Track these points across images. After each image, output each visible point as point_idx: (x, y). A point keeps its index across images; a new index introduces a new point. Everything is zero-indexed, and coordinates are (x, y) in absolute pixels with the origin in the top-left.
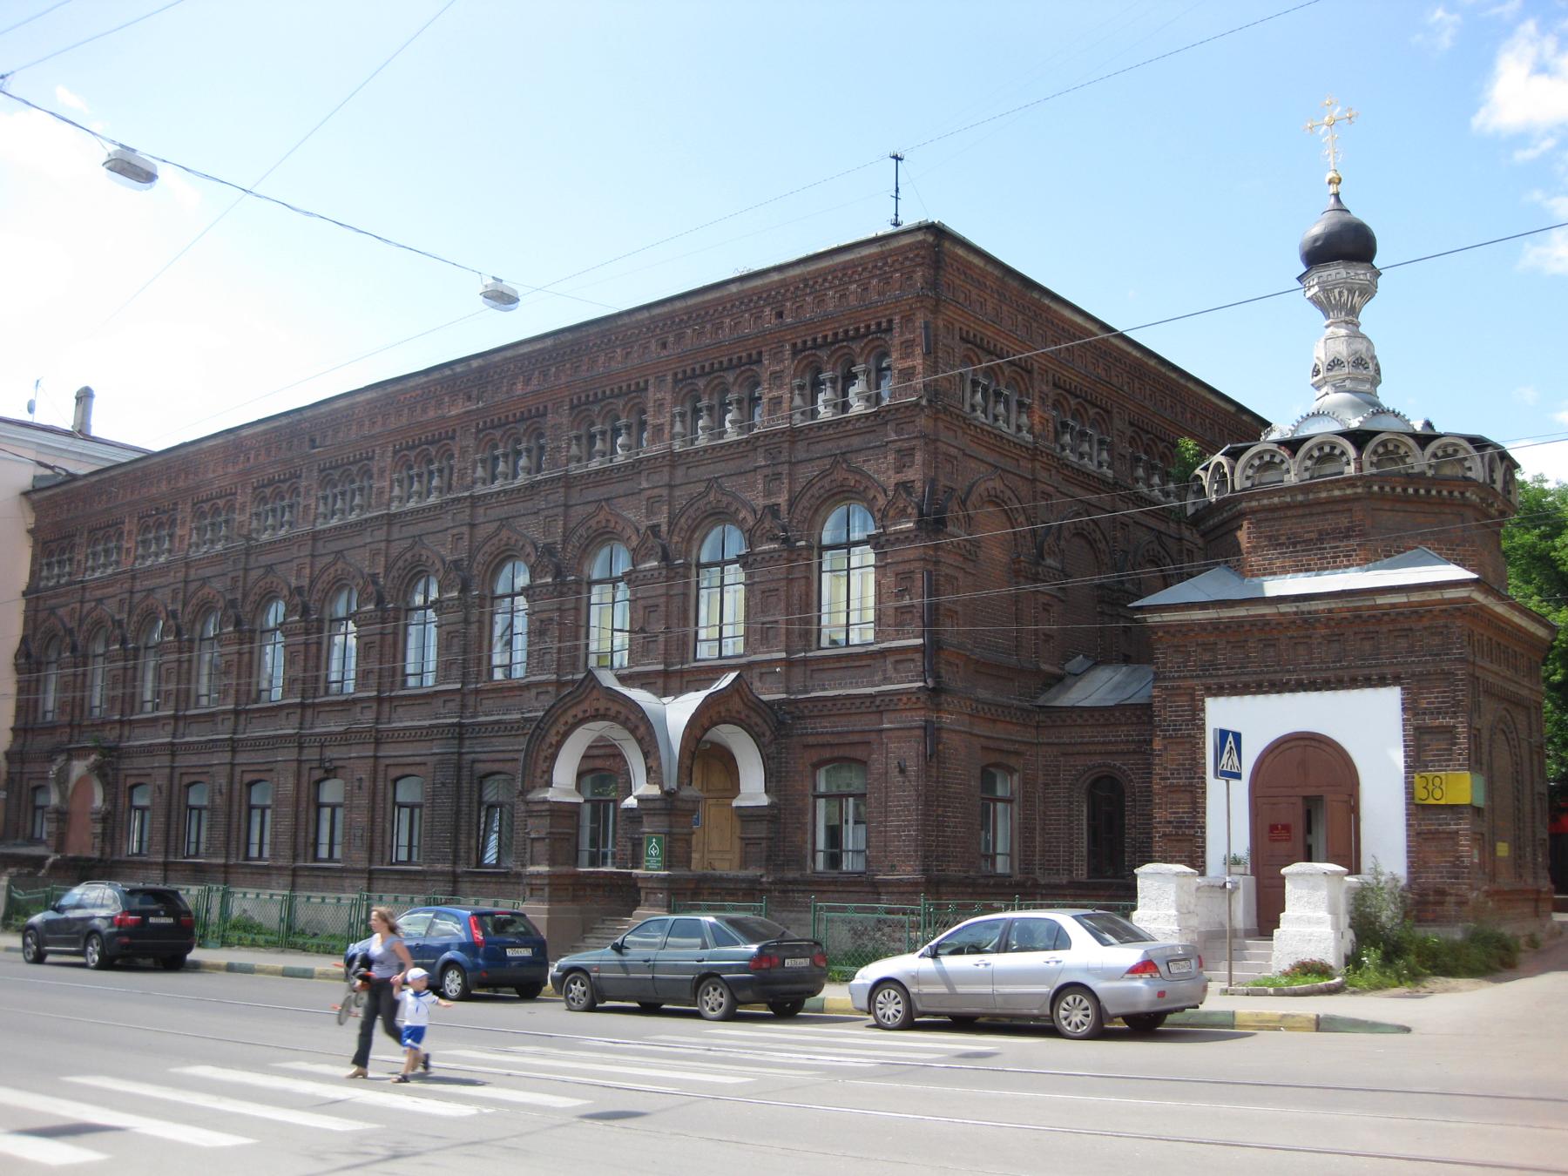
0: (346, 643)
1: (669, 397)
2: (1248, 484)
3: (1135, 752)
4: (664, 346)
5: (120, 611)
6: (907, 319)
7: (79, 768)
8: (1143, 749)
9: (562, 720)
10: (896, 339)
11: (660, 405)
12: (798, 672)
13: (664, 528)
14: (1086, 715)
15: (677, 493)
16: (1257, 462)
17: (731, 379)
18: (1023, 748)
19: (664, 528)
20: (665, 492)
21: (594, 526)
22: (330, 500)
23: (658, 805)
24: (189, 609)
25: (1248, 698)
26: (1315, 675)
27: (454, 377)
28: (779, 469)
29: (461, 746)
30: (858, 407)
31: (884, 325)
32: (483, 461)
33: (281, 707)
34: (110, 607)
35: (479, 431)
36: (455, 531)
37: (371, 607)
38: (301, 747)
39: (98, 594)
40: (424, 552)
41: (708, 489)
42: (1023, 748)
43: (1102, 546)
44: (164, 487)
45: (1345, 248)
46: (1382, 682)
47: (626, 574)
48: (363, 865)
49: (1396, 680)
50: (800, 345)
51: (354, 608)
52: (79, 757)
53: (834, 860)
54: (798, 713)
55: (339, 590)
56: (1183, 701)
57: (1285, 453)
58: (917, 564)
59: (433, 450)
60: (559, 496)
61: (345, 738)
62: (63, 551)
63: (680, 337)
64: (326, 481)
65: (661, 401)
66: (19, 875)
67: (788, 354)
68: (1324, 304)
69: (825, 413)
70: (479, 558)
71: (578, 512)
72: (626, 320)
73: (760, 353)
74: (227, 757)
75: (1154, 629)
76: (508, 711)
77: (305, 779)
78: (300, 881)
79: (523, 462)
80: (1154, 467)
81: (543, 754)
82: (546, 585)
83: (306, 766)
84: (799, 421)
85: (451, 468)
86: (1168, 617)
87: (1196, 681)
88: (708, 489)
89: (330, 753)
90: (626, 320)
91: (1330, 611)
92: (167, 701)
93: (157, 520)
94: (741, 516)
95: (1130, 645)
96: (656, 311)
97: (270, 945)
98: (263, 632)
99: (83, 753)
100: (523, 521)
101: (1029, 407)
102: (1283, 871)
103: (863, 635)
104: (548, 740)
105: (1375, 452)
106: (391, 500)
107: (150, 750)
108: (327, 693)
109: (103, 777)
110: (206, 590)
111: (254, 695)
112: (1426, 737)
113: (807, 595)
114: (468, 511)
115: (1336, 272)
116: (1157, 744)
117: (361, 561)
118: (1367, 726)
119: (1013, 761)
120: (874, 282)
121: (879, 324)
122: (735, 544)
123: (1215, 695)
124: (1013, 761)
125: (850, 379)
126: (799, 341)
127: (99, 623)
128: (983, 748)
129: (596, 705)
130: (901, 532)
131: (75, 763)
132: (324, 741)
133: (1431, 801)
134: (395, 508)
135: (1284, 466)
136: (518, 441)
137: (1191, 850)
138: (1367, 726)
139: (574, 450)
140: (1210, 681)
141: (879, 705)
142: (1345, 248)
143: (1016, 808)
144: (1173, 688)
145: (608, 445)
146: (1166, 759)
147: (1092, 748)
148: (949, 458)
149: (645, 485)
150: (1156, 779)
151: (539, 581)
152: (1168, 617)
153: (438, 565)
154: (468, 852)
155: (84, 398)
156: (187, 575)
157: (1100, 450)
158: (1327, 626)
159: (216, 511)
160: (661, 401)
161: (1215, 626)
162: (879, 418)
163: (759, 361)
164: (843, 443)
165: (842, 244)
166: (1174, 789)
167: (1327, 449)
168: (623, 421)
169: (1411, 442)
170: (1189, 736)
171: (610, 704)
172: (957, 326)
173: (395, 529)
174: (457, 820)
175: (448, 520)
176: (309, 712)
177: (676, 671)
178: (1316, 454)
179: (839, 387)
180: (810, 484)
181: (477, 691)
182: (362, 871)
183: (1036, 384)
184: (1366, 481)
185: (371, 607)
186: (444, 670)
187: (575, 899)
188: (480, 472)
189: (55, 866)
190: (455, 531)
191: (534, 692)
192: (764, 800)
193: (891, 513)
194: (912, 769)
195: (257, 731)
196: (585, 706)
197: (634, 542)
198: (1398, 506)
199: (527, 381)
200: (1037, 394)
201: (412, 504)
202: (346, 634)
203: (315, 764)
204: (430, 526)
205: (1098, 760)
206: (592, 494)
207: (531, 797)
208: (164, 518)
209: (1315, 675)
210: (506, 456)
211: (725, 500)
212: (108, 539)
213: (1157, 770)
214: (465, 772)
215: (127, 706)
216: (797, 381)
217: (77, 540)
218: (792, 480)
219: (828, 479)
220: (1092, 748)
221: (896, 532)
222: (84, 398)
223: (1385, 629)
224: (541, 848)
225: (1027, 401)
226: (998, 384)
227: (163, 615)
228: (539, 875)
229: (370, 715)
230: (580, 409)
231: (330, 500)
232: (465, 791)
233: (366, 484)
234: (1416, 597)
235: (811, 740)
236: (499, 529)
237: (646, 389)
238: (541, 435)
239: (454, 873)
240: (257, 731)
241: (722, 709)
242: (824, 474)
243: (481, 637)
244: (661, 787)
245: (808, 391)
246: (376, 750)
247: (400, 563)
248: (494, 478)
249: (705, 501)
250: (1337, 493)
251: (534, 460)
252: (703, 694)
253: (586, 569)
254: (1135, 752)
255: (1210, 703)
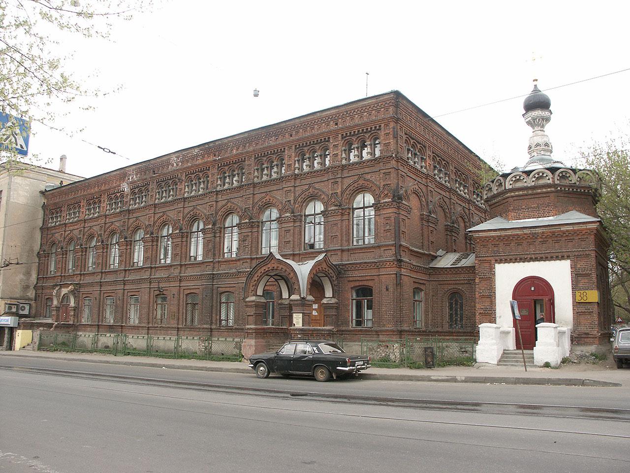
0: (115, 252)
1: (293, 154)
2: (511, 187)
3: (467, 283)
4: (291, 136)
5: (79, 235)
6: (387, 125)
7: (64, 291)
8: (471, 283)
9: (259, 271)
10: (382, 133)
11: (213, 175)
12: (345, 254)
13: (292, 202)
14: (448, 270)
15: (297, 189)
16: (514, 179)
17: (318, 148)
18: (425, 282)
19: (292, 202)
20: (292, 189)
21: (265, 201)
22: (161, 193)
23: (299, 302)
24: (107, 233)
25: (553, 262)
26: (537, 256)
27: (210, 148)
28: (337, 180)
29: (213, 282)
30: (235, 184)
31: (327, 139)
32: (220, 178)
33: (142, 268)
34: (76, 232)
35: (219, 168)
36: (210, 204)
37: (178, 231)
38: (150, 283)
39: (71, 228)
40: (198, 211)
41: (310, 187)
42: (425, 282)
43: (447, 211)
44: (96, 189)
45: (537, 104)
46: (563, 258)
47: (277, 218)
48: (175, 326)
49: (568, 257)
50: (345, 135)
51: (117, 241)
52: (64, 287)
53: (359, 323)
54: (346, 269)
55: (165, 225)
56: (487, 265)
57: (525, 175)
58: (392, 214)
59: (201, 174)
60: (251, 191)
61: (168, 279)
62: (57, 213)
63: (297, 132)
64: (159, 186)
65: (291, 156)
66: (44, 330)
67: (340, 138)
68: (532, 123)
69: (353, 159)
70: (220, 213)
71: (258, 197)
72: (277, 126)
73: (329, 138)
74: (98, 288)
75: (476, 239)
76: (231, 269)
77: (152, 294)
78: (150, 331)
79: (202, 186)
80: (461, 184)
81: (252, 284)
82: (246, 223)
83: (126, 291)
84: (344, 162)
85: (208, 181)
86: (481, 234)
87: (492, 258)
88: (310, 187)
89: (161, 285)
90: (277, 126)
91: (543, 232)
92: (98, 266)
93: (94, 201)
94: (323, 197)
95: (470, 243)
96: (302, 120)
97: (397, 367)
98: (224, 228)
99: (67, 285)
100: (236, 200)
101: (425, 159)
102: (536, 326)
103: (369, 240)
104: (254, 279)
105: (559, 175)
106: (185, 192)
107: (91, 284)
108: (160, 263)
109: (74, 294)
110: (113, 226)
111: (132, 264)
112: (580, 278)
113: (300, 232)
114: (215, 197)
115: (538, 113)
116: (477, 281)
117: (240, 203)
118: (558, 274)
119: (422, 287)
120: (374, 112)
121: (376, 127)
122: (369, 199)
123: (499, 263)
124: (422, 287)
125: (363, 146)
126: (344, 134)
127: (71, 239)
128: (414, 282)
129: (273, 265)
130: (386, 202)
131: (63, 289)
132: (159, 280)
133: (582, 301)
134: (186, 195)
135: (525, 180)
136: (234, 171)
137: (551, 318)
138: (558, 274)
139: (256, 174)
140: (497, 258)
141: (377, 265)
142: (537, 104)
143: (423, 304)
144: (483, 260)
145: (269, 172)
146: (480, 288)
147: (450, 282)
148: (402, 176)
149: (284, 186)
150: (477, 293)
151: (207, 227)
152: (481, 234)
153: (203, 216)
154: (216, 321)
155: (63, 159)
156: (106, 221)
157: (446, 177)
158: (541, 238)
159: (117, 198)
160: (291, 156)
161: (575, 232)
162: (375, 161)
163: (328, 141)
164: (362, 170)
165: (361, 98)
166: (483, 297)
167: (541, 174)
168: (227, 174)
169: (571, 172)
170: (489, 278)
171: (279, 265)
172: (404, 128)
173: (186, 203)
174: (212, 309)
175: (207, 200)
176: (183, 268)
177: (297, 254)
178: (537, 176)
179: (360, 150)
180: (350, 185)
181: (219, 262)
182: (175, 328)
183: (427, 151)
184: (554, 185)
185: (178, 231)
186: (205, 254)
187: (263, 338)
188: (219, 182)
189: (56, 327)
190: (210, 204)
191: (242, 262)
192: (334, 301)
193: (382, 196)
194: (391, 289)
195: (131, 277)
196: (269, 266)
197: (280, 207)
198: (566, 195)
199: (237, 150)
200: (427, 155)
201: (193, 194)
202: (115, 249)
203: (157, 289)
204: (200, 202)
205: (452, 286)
206: (263, 190)
207: (247, 300)
208: (97, 200)
209: (537, 256)
210: (229, 176)
211: (316, 191)
212: (75, 208)
213: (477, 290)
214: (215, 292)
215: (63, 270)
216: (344, 148)
217: (63, 209)
218: (342, 184)
219: (357, 183)
220: (450, 282)
221: (384, 202)
222: (63, 159)
223: (564, 239)
224: (251, 319)
225: (425, 157)
226: (415, 151)
227: (96, 235)
228: (251, 329)
229: (177, 271)
230: (259, 160)
231: (161, 193)
232: (215, 299)
233: (174, 187)
234: (576, 227)
235: (351, 279)
236: (227, 203)
237: (284, 152)
238: (243, 169)
239: (211, 329)
240: (131, 277)
241: (320, 267)
242: (355, 182)
243: (220, 243)
244: (300, 296)
245: (347, 152)
246: (180, 284)
247: (189, 216)
248: (135, 204)
249: (308, 191)
250: (544, 190)
251: (240, 178)
252: (315, 261)
253: (261, 217)
254: (467, 283)
255: (497, 265)
